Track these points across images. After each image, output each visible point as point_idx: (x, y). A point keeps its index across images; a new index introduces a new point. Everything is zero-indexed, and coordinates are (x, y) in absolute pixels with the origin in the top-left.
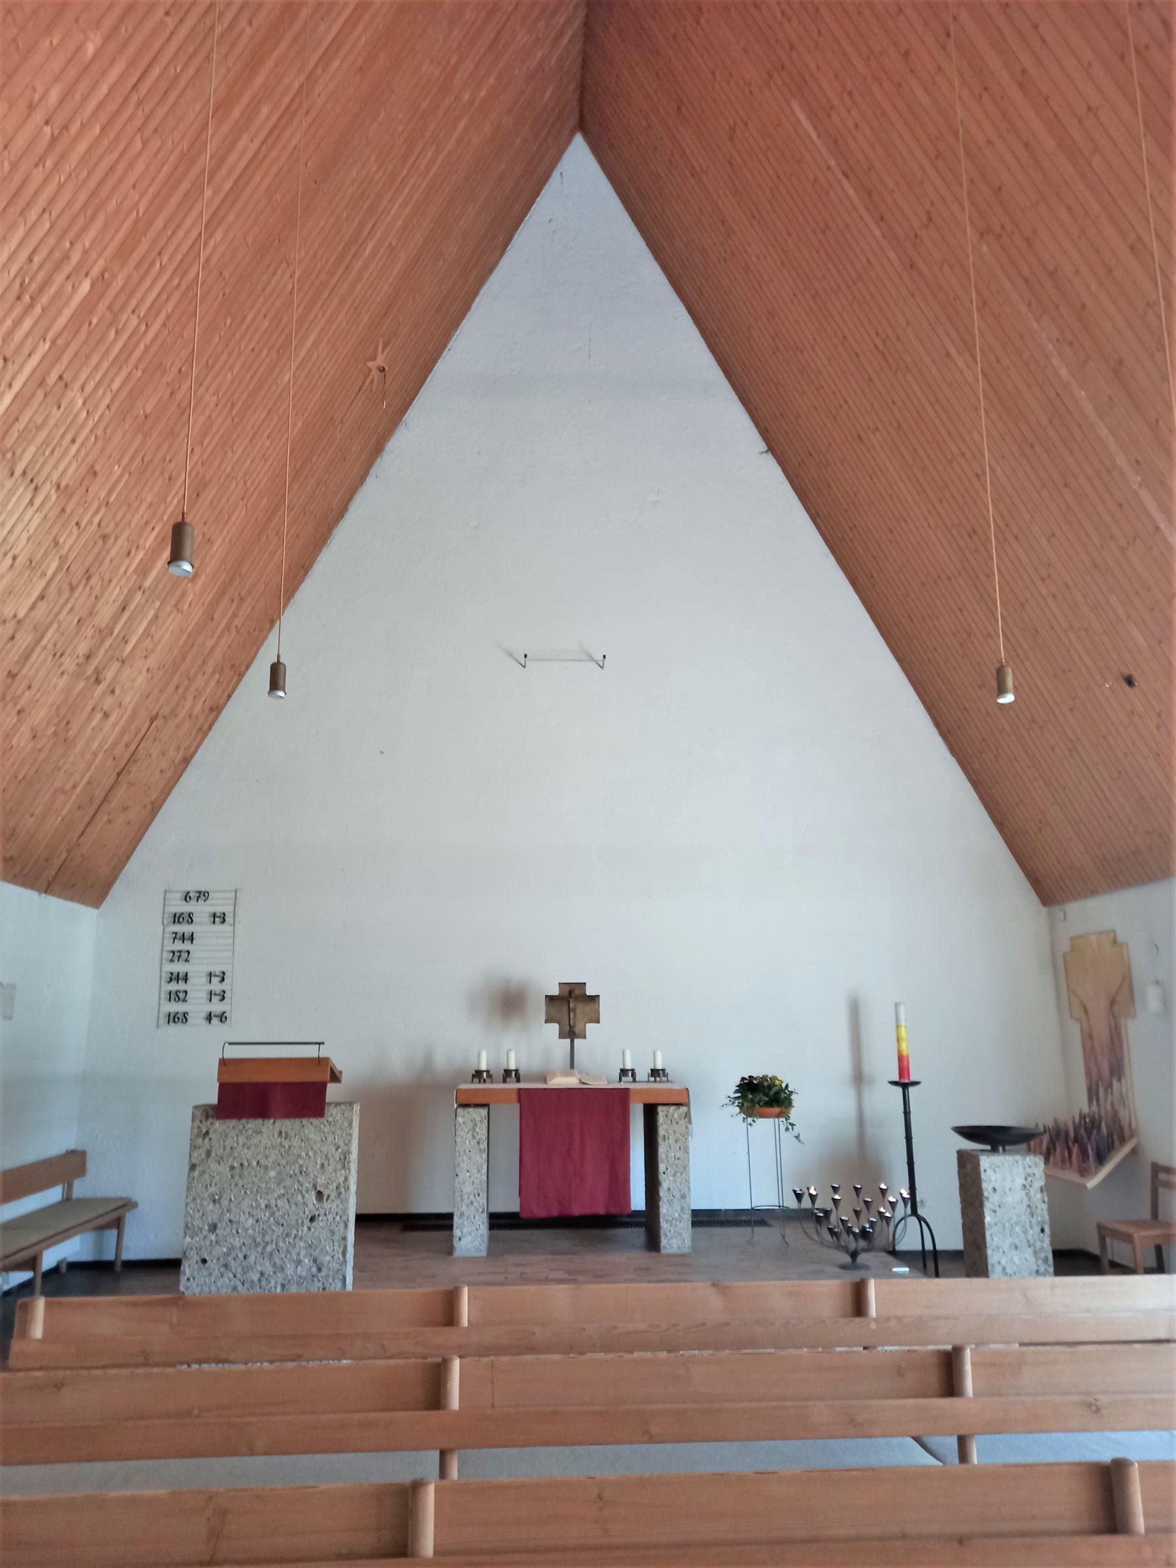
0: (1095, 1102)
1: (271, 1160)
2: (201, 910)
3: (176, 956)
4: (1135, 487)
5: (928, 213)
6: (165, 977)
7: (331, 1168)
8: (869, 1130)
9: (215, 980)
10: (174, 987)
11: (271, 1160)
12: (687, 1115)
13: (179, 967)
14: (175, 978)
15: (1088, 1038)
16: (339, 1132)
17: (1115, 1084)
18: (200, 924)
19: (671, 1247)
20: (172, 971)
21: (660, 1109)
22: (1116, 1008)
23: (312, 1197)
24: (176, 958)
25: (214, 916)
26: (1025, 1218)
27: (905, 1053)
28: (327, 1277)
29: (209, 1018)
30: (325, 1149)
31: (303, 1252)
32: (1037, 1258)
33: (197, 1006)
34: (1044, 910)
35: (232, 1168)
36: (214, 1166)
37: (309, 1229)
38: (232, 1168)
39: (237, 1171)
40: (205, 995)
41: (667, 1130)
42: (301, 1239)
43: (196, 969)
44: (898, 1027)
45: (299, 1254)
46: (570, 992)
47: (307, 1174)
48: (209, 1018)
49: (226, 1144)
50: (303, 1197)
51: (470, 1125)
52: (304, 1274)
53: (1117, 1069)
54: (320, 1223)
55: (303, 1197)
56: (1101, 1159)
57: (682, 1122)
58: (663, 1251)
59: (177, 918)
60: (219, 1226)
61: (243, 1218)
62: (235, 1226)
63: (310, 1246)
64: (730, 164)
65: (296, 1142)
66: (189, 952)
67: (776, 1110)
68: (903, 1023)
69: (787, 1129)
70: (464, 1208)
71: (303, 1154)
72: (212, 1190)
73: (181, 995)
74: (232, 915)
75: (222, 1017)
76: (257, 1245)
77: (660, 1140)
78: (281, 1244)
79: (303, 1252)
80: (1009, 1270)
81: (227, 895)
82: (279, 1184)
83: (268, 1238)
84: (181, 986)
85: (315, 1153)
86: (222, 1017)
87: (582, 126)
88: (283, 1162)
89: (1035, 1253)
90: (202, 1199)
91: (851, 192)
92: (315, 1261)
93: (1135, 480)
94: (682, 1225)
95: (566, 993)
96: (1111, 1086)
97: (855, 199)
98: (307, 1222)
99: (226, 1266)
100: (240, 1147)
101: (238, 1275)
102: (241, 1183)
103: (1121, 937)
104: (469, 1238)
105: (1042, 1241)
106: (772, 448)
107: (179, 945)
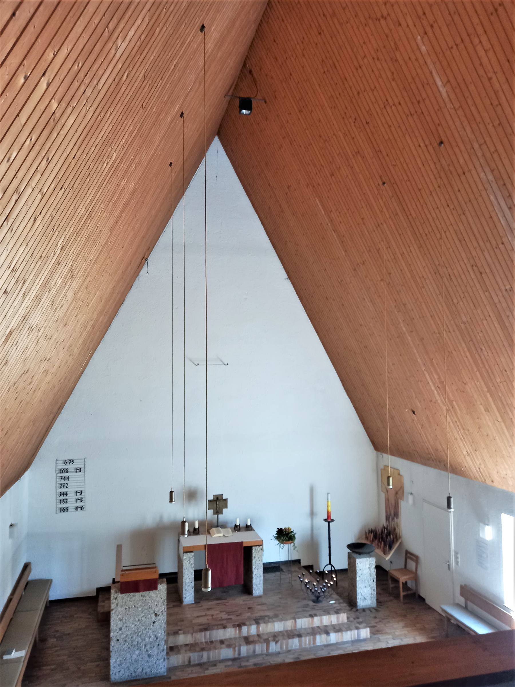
0: (388, 522)
1: (139, 604)
2: (71, 467)
3: (62, 485)
4: (423, 370)
5: (364, 261)
6: (59, 494)
7: (159, 605)
8: (315, 531)
9: (78, 494)
10: (62, 497)
11: (139, 604)
12: (262, 549)
13: (64, 490)
14: (62, 494)
15: (387, 500)
16: (162, 593)
17: (395, 519)
18: (71, 472)
19: (256, 593)
20: (61, 491)
21: (254, 548)
22: (398, 495)
23: (153, 616)
24: (62, 487)
25: (77, 469)
26: (369, 578)
27: (330, 511)
28: (160, 641)
29: (77, 509)
30: (157, 599)
31: (151, 634)
32: (371, 590)
33: (71, 504)
34: (375, 452)
35: (126, 609)
36: (119, 609)
37: (153, 626)
38: (126, 609)
39: (128, 610)
40: (74, 500)
41: (255, 555)
42: (150, 629)
43: (70, 490)
44: (328, 502)
45: (150, 635)
46: (217, 498)
47: (152, 608)
48: (77, 509)
49: (124, 601)
50: (151, 616)
51: (188, 559)
52: (152, 641)
53: (396, 514)
54: (157, 624)
55: (151, 616)
56: (390, 548)
57: (261, 551)
58: (254, 595)
59: (62, 471)
60: (123, 628)
61: (130, 625)
62: (128, 628)
63: (154, 631)
64: (287, 195)
65: (147, 598)
66: (67, 484)
67: (291, 542)
68: (330, 501)
69: (294, 549)
70: (186, 587)
71: (150, 602)
72: (119, 617)
73: (65, 501)
74: (83, 468)
75: (82, 508)
76: (136, 633)
77: (253, 558)
78: (144, 632)
79: (151, 634)
80: (363, 594)
81: (81, 461)
82: (142, 612)
83: (139, 630)
84: (65, 497)
85: (154, 601)
86: (82, 508)
87: (219, 134)
88: (143, 605)
89: (371, 588)
90: (116, 620)
91: (335, 236)
92: (155, 636)
93: (424, 368)
94: (260, 586)
95: (216, 499)
96: (394, 519)
97: (336, 238)
98: (152, 624)
99: (126, 641)
100: (128, 602)
101: (130, 643)
102: (129, 613)
103: (401, 473)
104: (188, 597)
105: (373, 584)
106: (289, 277)
107: (63, 481)
